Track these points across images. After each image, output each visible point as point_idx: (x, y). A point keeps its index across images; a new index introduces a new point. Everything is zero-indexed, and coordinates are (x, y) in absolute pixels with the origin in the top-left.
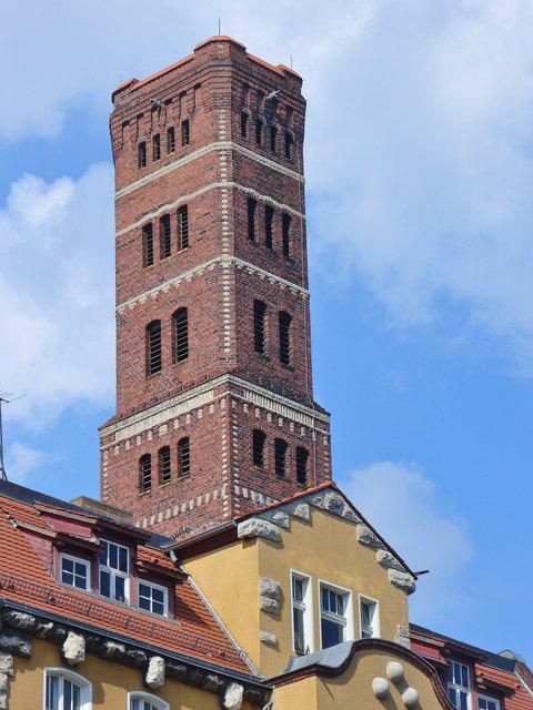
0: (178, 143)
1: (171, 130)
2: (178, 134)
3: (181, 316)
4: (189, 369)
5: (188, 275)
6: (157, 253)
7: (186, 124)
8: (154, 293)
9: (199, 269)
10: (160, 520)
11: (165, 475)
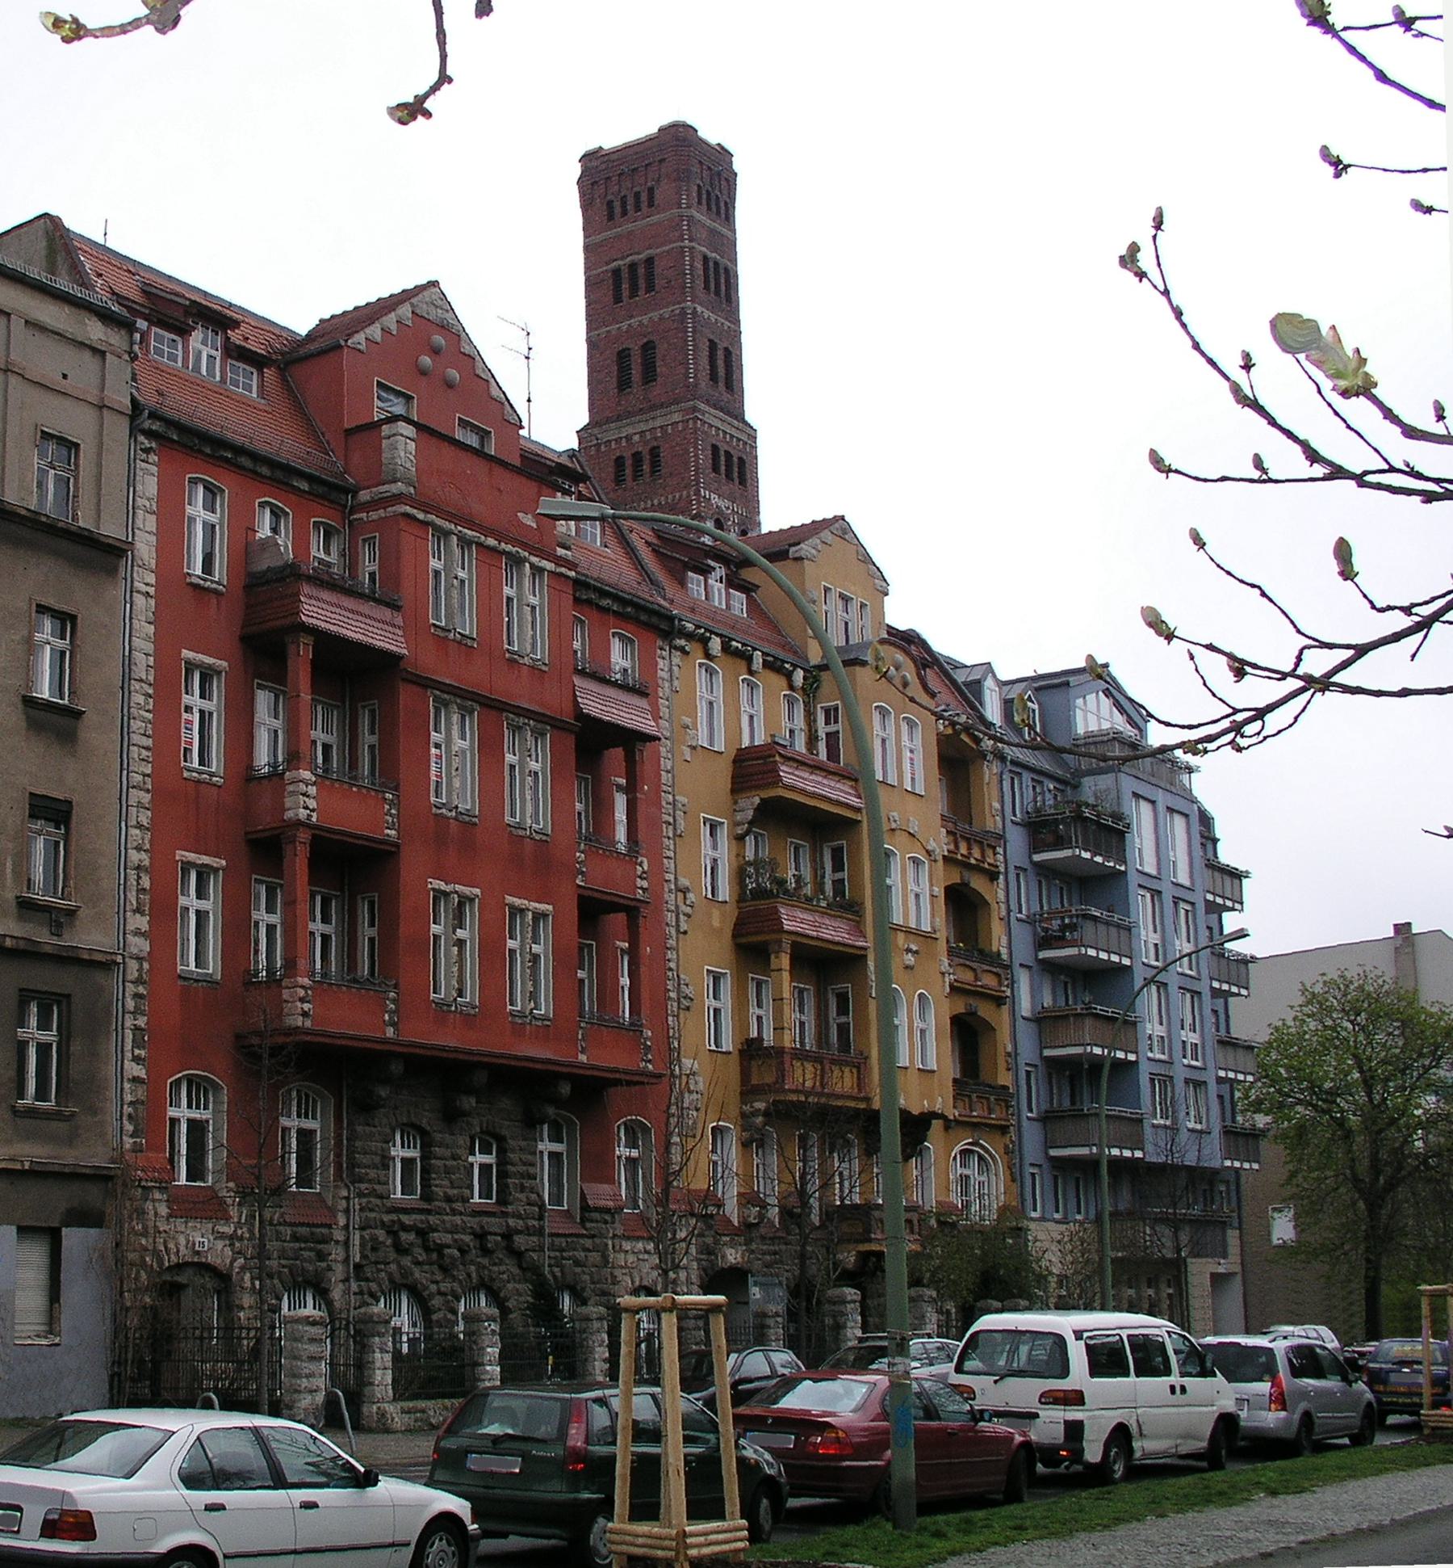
0: (644, 205)
1: (637, 195)
2: (644, 197)
3: (648, 348)
4: (657, 391)
5: (655, 315)
6: (625, 293)
7: (651, 190)
8: (624, 326)
9: (666, 312)
10: (645, 884)
11: (634, 292)
